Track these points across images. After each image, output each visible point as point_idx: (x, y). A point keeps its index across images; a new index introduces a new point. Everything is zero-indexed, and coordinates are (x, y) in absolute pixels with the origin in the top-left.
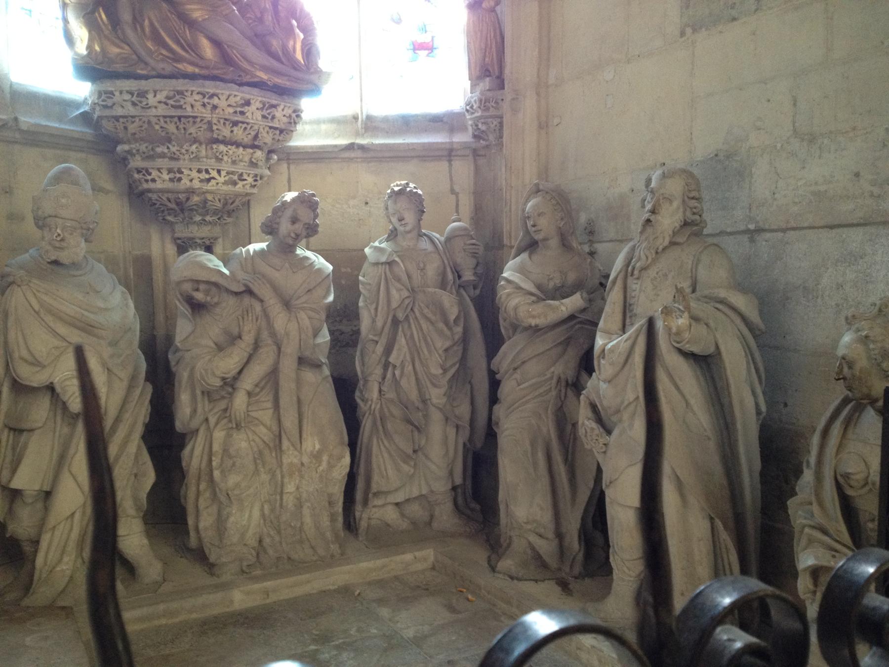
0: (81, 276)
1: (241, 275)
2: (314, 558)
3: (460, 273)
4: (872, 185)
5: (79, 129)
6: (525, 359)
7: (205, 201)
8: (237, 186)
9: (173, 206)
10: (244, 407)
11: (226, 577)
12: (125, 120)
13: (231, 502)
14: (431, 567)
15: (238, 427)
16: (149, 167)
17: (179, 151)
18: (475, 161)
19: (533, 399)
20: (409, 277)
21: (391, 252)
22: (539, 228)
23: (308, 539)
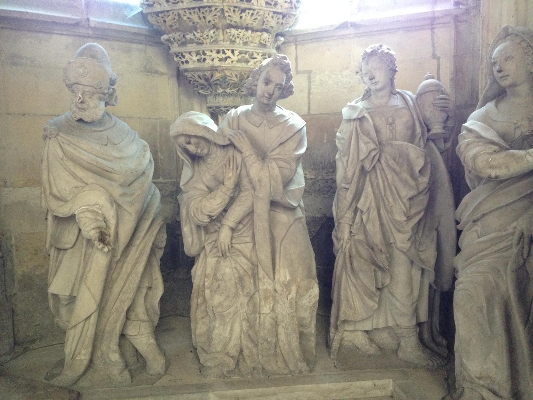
0: (102, 131)
1: (228, 132)
2: (286, 371)
3: (429, 127)
5: (140, 26)
6: (485, 212)
7: (225, 77)
8: (249, 64)
9: (203, 81)
10: (228, 240)
11: (210, 379)
12: (163, 14)
13: (216, 318)
14: (390, 395)
15: (224, 255)
16: (183, 51)
17: (202, 36)
18: (456, 27)
19: (492, 253)
20: (377, 131)
21: (362, 108)
22: (506, 73)
23: (282, 353)
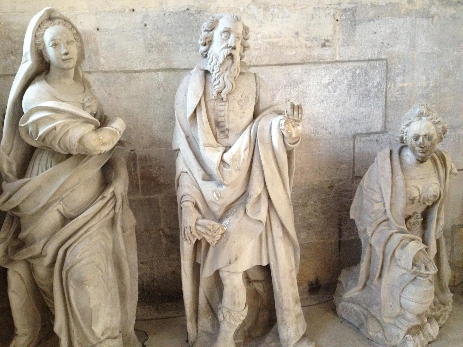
4: (306, 41)
